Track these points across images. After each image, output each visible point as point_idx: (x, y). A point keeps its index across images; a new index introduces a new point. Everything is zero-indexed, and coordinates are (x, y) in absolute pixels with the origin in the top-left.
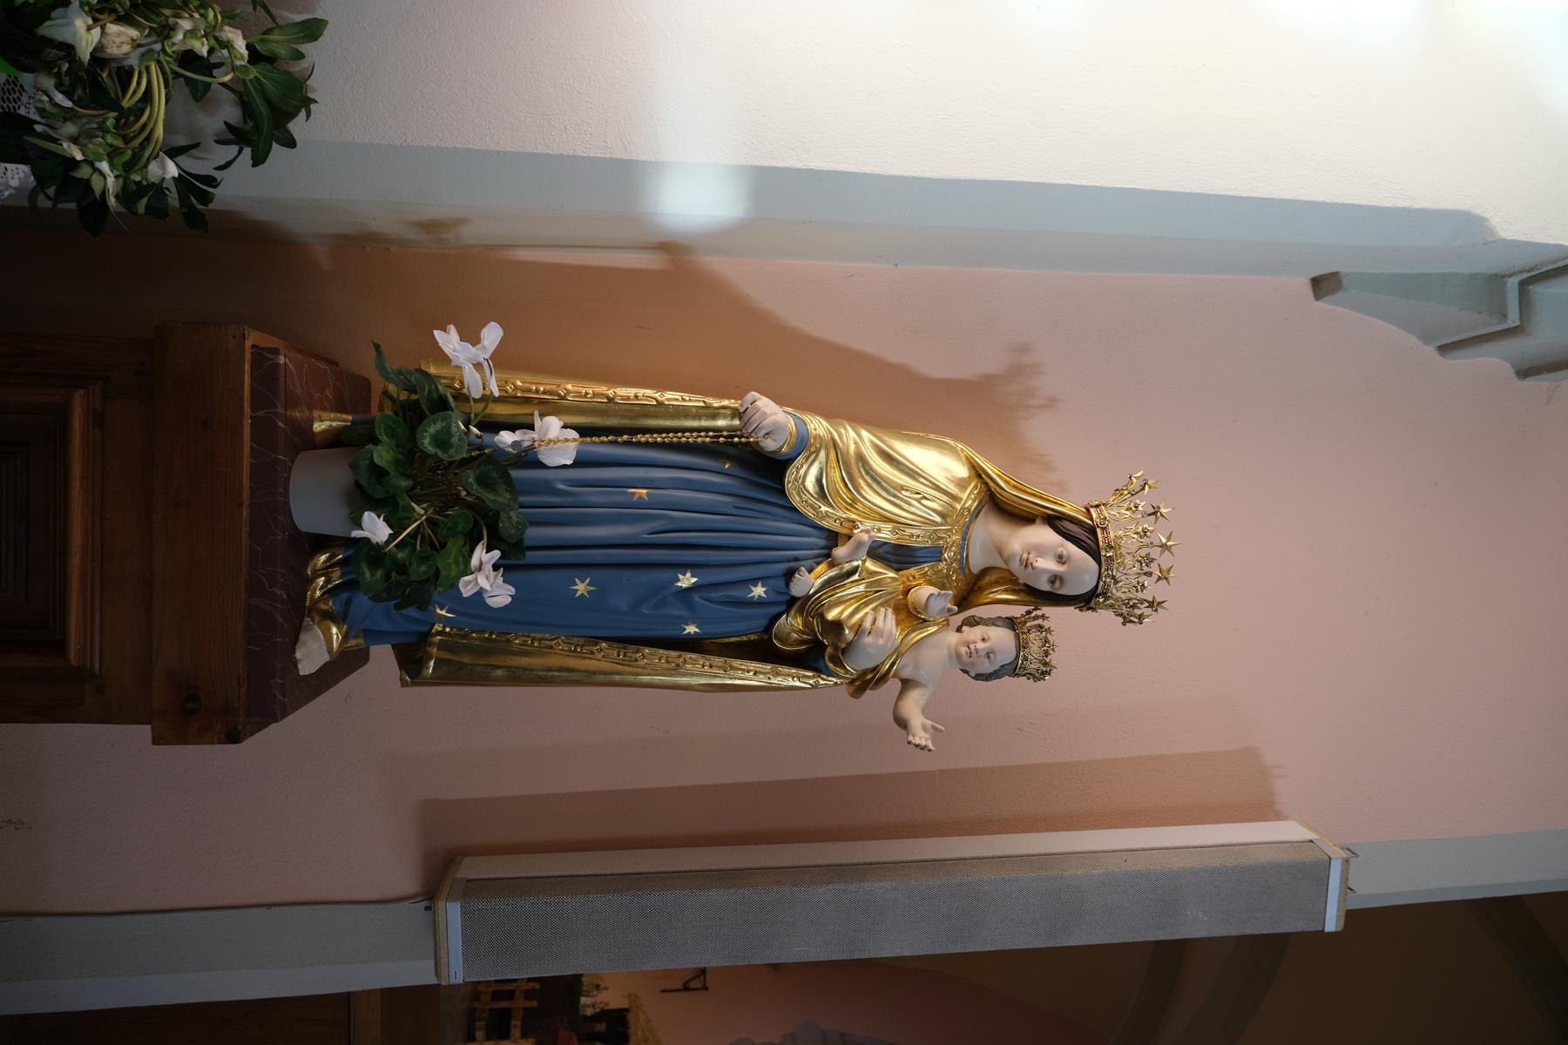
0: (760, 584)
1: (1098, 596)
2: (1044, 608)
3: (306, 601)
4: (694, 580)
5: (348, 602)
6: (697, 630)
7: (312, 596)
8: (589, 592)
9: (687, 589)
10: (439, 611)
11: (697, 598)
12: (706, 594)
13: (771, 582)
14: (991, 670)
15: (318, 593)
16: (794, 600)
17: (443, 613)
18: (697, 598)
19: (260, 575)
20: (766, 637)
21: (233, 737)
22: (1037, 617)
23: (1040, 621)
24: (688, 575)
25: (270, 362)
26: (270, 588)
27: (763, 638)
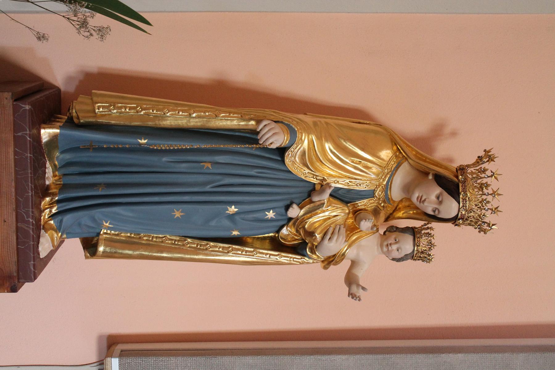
0: (271, 211)
1: (459, 219)
2: (433, 223)
3: (41, 221)
4: (236, 210)
5: (61, 221)
6: (239, 233)
7: (44, 219)
8: (181, 216)
9: (233, 214)
10: (105, 224)
11: (237, 218)
12: (243, 216)
13: (277, 209)
14: (400, 257)
15: (47, 217)
16: (290, 219)
17: (107, 224)
18: (237, 218)
19: (22, 212)
20: (277, 235)
21: (14, 290)
22: (428, 228)
23: (429, 231)
24: (233, 207)
25: (23, 109)
26: (27, 218)
27: (275, 236)
